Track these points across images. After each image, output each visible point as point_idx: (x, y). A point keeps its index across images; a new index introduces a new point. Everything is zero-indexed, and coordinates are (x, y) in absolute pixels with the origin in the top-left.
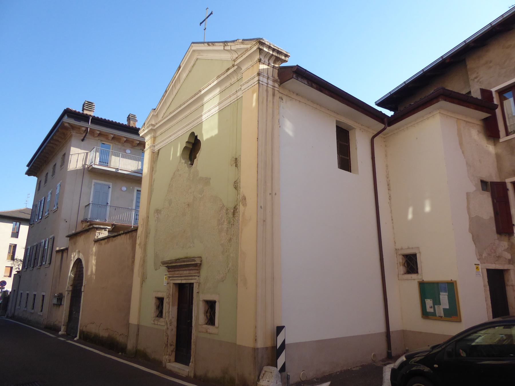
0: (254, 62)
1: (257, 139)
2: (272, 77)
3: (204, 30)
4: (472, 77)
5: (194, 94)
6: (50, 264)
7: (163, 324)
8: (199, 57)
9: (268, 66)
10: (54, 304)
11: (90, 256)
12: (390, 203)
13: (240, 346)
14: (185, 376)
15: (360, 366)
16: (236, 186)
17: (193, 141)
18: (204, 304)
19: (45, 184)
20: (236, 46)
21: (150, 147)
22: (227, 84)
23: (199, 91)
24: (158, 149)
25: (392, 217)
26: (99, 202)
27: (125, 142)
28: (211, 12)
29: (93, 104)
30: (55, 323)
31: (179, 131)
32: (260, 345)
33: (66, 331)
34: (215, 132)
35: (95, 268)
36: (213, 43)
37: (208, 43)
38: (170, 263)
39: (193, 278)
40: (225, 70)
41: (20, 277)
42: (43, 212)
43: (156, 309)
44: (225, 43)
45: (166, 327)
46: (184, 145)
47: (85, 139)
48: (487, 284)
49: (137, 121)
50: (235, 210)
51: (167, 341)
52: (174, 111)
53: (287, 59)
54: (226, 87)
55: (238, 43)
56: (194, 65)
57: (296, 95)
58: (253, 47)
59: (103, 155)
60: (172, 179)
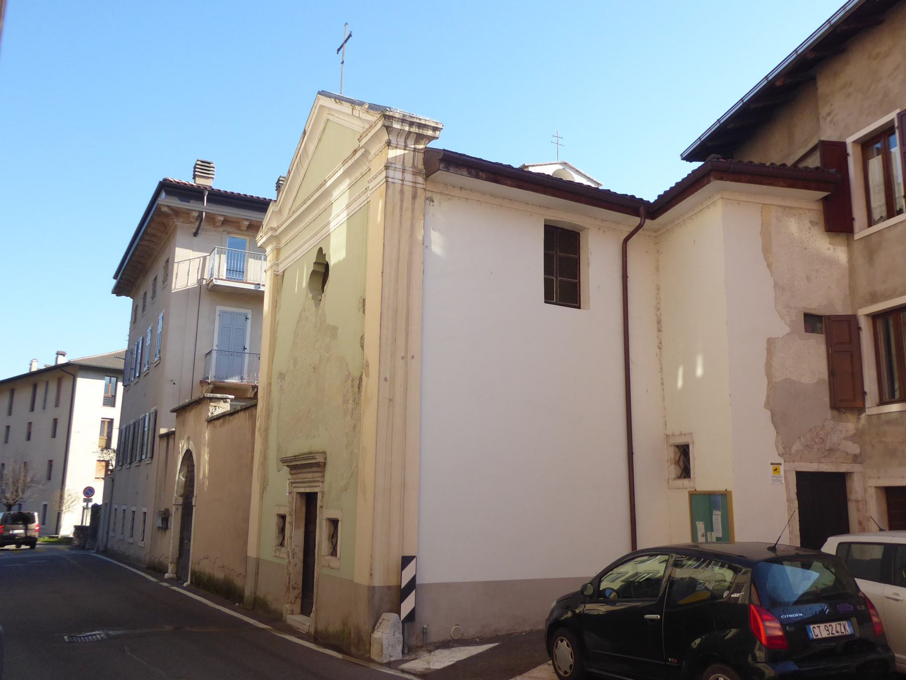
4: (824, 111)
6: (152, 458)
7: (285, 556)
9: (405, 149)
10: (159, 527)
12: (659, 356)
13: (357, 584)
19: (143, 311)
22: (357, 174)
24: (283, 270)
25: (662, 379)
26: (229, 348)
29: (212, 165)
30: (161, 560)
32: (378, 582)
33: (176, 573)
39: (314, 484)
40: (352, 153)
41: (113, 481)
42: (141, 364)
43: (279, 533)
45: (287, 561)
47: (199, 231)
48: (794, 497)
51: (289, 583)
56: (324, 129)
57: (460, 189)
59: (234, 261)
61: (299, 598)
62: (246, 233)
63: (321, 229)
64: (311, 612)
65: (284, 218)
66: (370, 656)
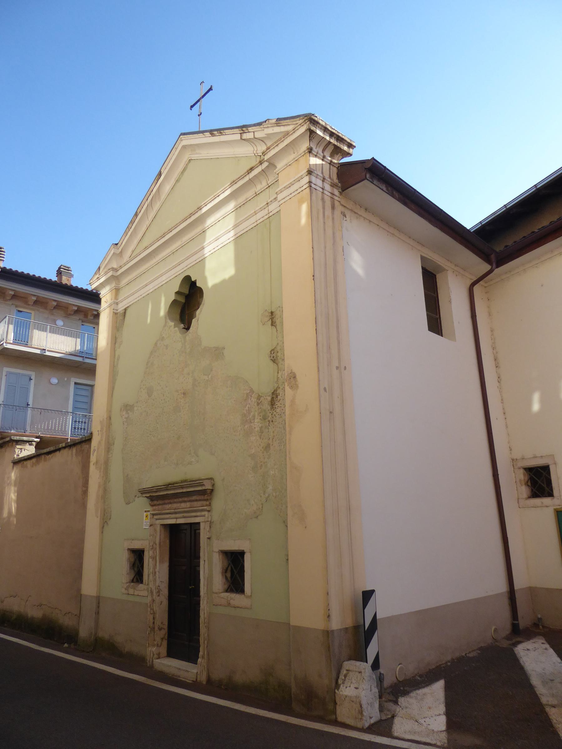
0: (299, 153)
1: (313, 276)
2: (329, 178)
3: (199, 115)
5: (188, 214)
7: (145, 593)
8: (194, 157)
9: (323, 160)
11: (6, 488)
14: (191, 682)
15: (477, 649)
16: (273, 357)
17: (186, 291)
18: (221, 556)
20: (266, 130)
21: (110, 305)
22: (250, 194)
23: (198, 208)
24: (124, 308)
27: (55, 308)
28: (210, 87)
31: (161, 275)
32: (336, 624)
34: (230, 272)
35: (16, 505)
36: (220, 131)
37: (211, 132)
38: (156, 492)
39: (198, 514)
43: (130, 568)
44: (243, 128)
45: (150, 598)
46: (173, 297)
49: (72, 276)
50: (274, 396)
51: (154, 623)
52: (151, 245)
53: (351, 151)
54: (247, 199)
55: (269, 126)
56: (184, 170)
57: (365, 211)
58: (298, 129)
60: (151, 353)
61: (166, 640)
62: (32, 307)
63: (196, 253)
64: (198, 657)
65: (125, 261)
66: (336, 718)
